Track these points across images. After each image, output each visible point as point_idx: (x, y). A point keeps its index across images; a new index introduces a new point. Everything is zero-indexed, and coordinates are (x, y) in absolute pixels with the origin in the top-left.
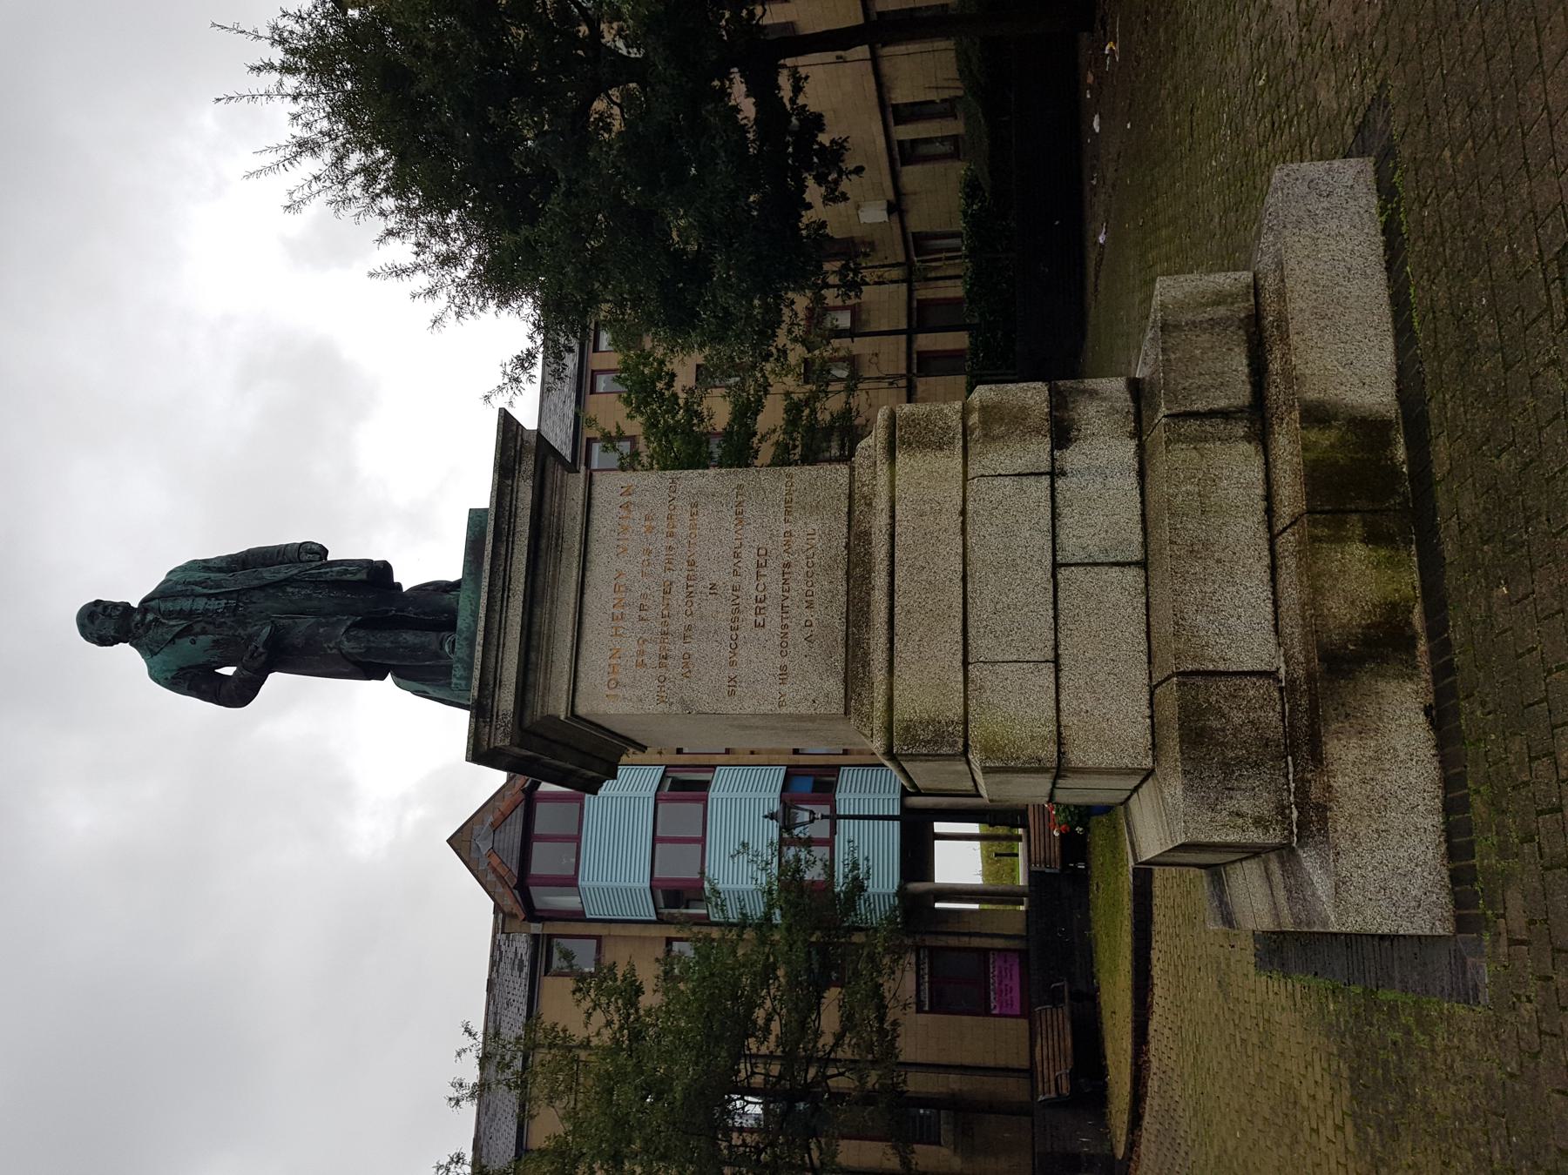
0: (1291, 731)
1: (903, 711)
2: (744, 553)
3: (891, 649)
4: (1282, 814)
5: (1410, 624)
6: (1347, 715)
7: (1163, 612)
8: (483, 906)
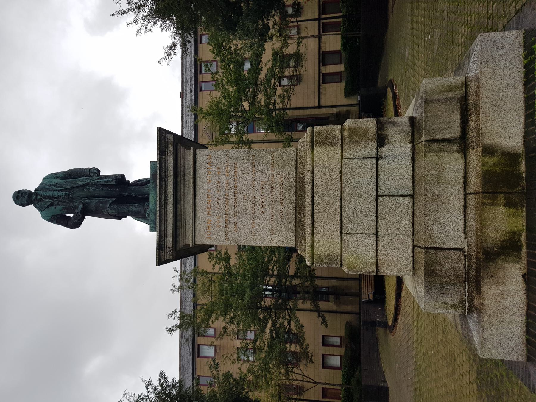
0: (468, 273)
1: (318, 250)
3: (313, 226)
4: (462, 303)
5: (520, 240)
6: (492, 276)
7: (419, 220)
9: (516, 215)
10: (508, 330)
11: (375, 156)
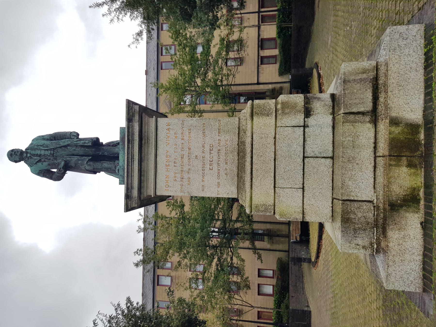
0: (376, 221)
1: (255, 201)
4: (371, 245)
5: (418, 195)
6: (396, 224)
9: (415, 174)
10: (408, 267)
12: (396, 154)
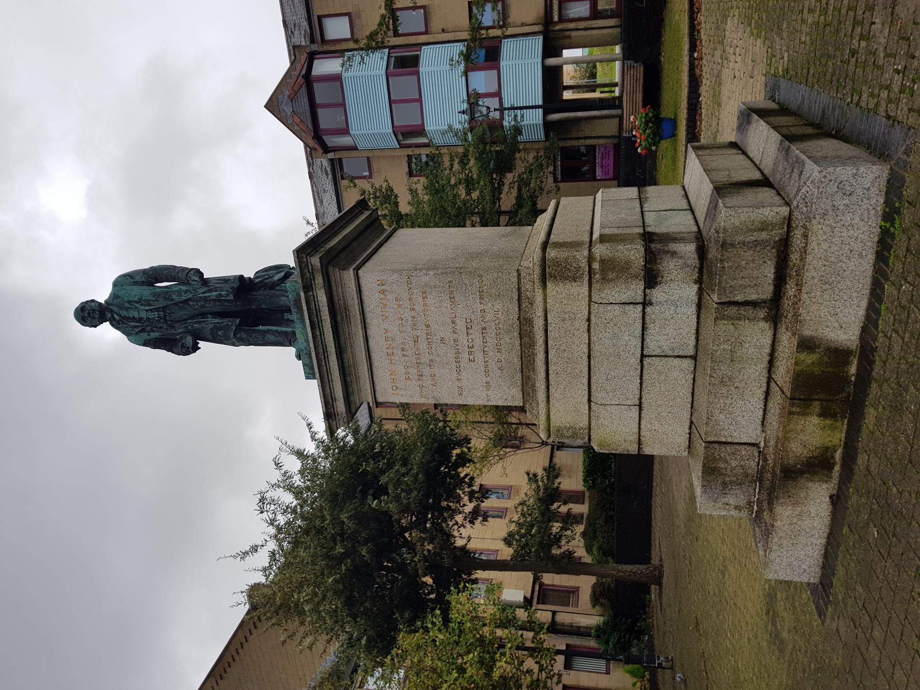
1: (556, 421)
2: (457, 321)
5: (833, 457)
8: (284, 64)
9: (832, 428)
10: (803, 552)
11: (641, 301)
12: (802, 397)
